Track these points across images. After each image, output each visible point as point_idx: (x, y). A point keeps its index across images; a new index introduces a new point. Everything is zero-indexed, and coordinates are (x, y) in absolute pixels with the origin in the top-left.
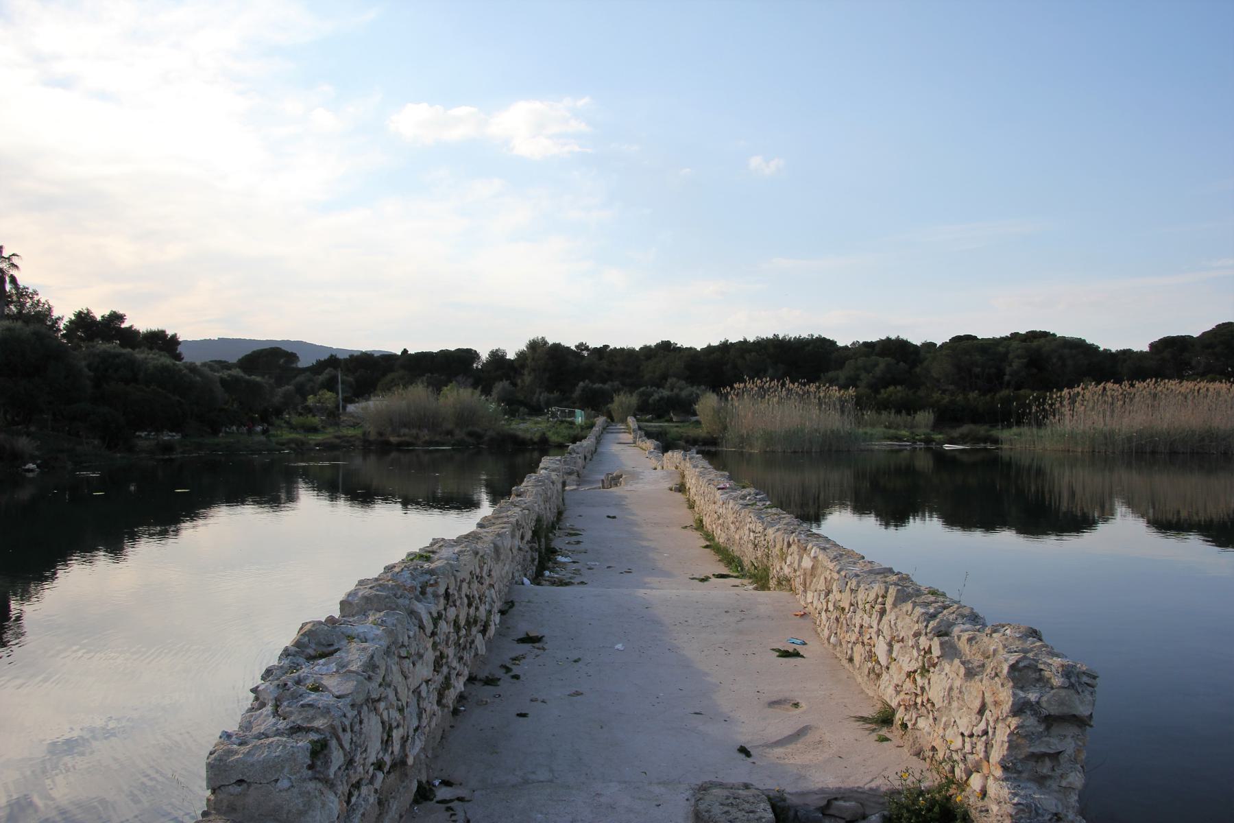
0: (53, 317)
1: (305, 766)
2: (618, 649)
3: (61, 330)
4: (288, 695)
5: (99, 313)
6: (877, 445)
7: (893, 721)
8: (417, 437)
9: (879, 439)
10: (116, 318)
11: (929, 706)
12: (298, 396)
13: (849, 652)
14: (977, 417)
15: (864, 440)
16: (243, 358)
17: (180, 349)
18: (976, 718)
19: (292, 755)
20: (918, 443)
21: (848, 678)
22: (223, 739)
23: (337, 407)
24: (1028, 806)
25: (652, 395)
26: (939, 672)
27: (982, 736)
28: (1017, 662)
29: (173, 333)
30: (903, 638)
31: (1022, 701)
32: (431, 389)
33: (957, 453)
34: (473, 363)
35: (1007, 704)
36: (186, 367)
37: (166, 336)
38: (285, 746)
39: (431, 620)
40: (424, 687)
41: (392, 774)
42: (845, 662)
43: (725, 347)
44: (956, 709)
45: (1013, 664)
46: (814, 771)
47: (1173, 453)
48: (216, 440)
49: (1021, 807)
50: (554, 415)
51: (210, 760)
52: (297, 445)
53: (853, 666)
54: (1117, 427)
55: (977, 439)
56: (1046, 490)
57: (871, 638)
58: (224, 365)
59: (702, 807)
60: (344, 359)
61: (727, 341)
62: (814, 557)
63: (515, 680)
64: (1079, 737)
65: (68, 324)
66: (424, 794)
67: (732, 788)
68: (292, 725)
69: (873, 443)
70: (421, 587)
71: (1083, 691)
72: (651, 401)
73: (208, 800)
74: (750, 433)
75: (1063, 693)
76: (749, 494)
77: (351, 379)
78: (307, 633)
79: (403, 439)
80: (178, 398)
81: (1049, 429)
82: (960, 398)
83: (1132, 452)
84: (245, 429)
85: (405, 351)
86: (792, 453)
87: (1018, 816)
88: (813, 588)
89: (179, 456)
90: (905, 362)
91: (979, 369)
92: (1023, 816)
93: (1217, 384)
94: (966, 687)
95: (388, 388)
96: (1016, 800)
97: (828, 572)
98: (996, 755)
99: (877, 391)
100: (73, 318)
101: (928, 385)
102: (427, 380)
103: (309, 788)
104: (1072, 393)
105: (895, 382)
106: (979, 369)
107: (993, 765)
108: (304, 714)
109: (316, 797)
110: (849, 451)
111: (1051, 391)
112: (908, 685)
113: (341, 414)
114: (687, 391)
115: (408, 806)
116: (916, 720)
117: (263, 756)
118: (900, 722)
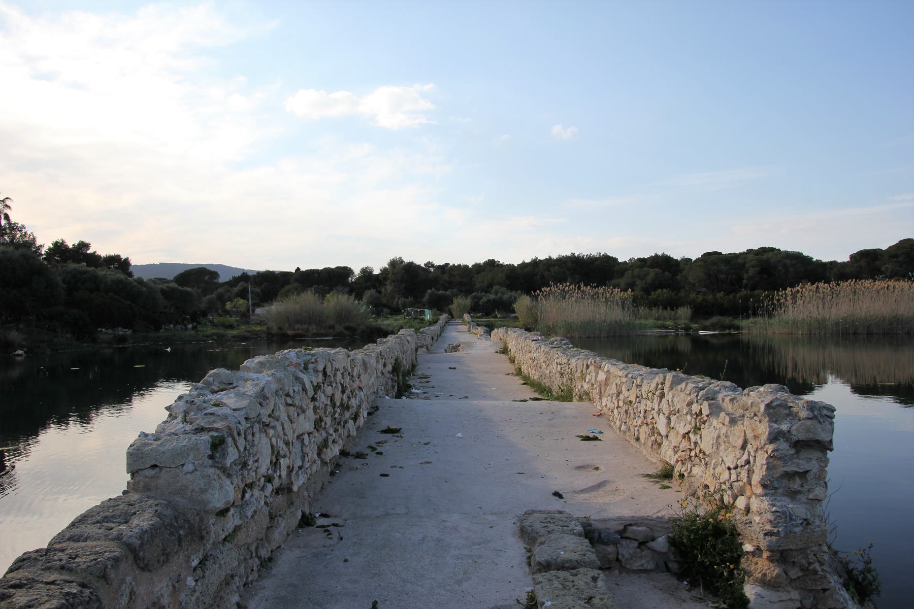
0: (37, 245)
1: (206, 455)
2: (458, 437)
3: (43, 255)
4: (194, 408)
5: (71, 242)
6: (649, 332)
7: (672, 475)
8: (307, 331)
9: (651, 328)
10: (83, 246)
11: (701, 455)
12: (219, 302)
13: (636, 434)
14: (722, 311)
15: (640, 329)
16: (178, 276)
17: (131, 269)
18: (740, 453)
19: (196, 445)
20: (680, 330)
21: (636, 452)
22: (141, 437)
23: (248, 310)
24: (784, 513)
25: (482, 298)
26: (708, 427)
27: (745, 466)
28: (772, 402)
29: (126, 257)
30: (679, 410)
31: (776, 431)
32: (317, 295)
33: (709, 338)
34: (349, 277)
35: (765, 434)
36: (135, 281)
37: (121, 259)
38: (190, 439)
39: (312, 387)
40: (306, 436)
41: (280, 496)
42: (633, 442)
43: (535, 263)
44: (723, 450)
45: (768, 403)
46: (613, 506)
47: (870, 334)
48: (158, 334)
49: (778, 514)
50: (409, 314)
51: (130, 450)
52: (218, 337)
53: (640, 444)
54: (828, 315)
55: (724, 327)
56: (776, 364)
57: (653, 418)
58: (163, 281)
59: (526, 523)
60: (253, 276)
61: (537, 258)
62: (608, 371)
63: (379, 455)
64: (822, 459)
65: (47, 251)
66: (306, 521)
67: (549, 513)
68: (197, 427)
69: (647, 331)
70: (304, 364)
71: (824, 422)
72: (481, 303)
73: (128, 483)
74: (555, 324)
75: (809, 422)
76: (556, 341)
77: (258, 290)
78: (213, 375)
79: (297, 332)
80: (129, 302)
81: (777, 318)
82: (710, 297)
83: (839, 334)
84: (179, 327)
85: (298, 269)
86: (586, 337)
87: (776, 522)
88: (607, 394)
89: (130, 345)
90: (669, 271)
91: (724, 276)
92: (780, 521)
93: (902, 283)
94: (731, 431)
95: (286, 295)
96: (774, 509)
97: (618, 378)
98: (756, 478)
99: (649, 294)
100: (52, 246)
101: (686, 289)
102: (315, 290)
103: (209, 472)
104: (793, 291)
105: (661, 286)
106: (724, 276)
107: (754, 486)
108: (207, 420)
109: (215, 480)
110: (628, 336)
111: (778, 291)
112: (684, 444)
113: (251, 315)
114: (508, 295)
115: (294, 528)
116: (691, 469)
117: (172, 446)
118: (678, 474)
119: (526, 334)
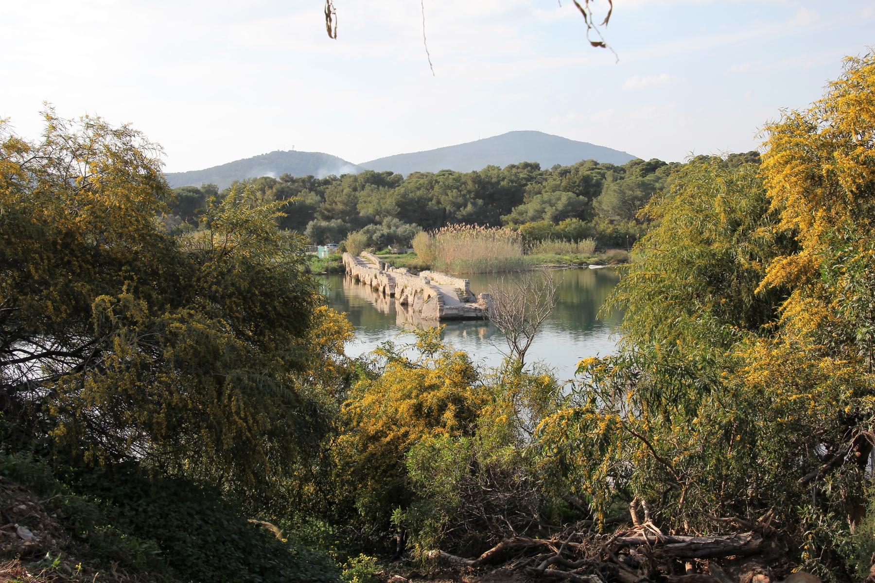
72: (374, 238)
101: (601, 216)
119: (13, 563)
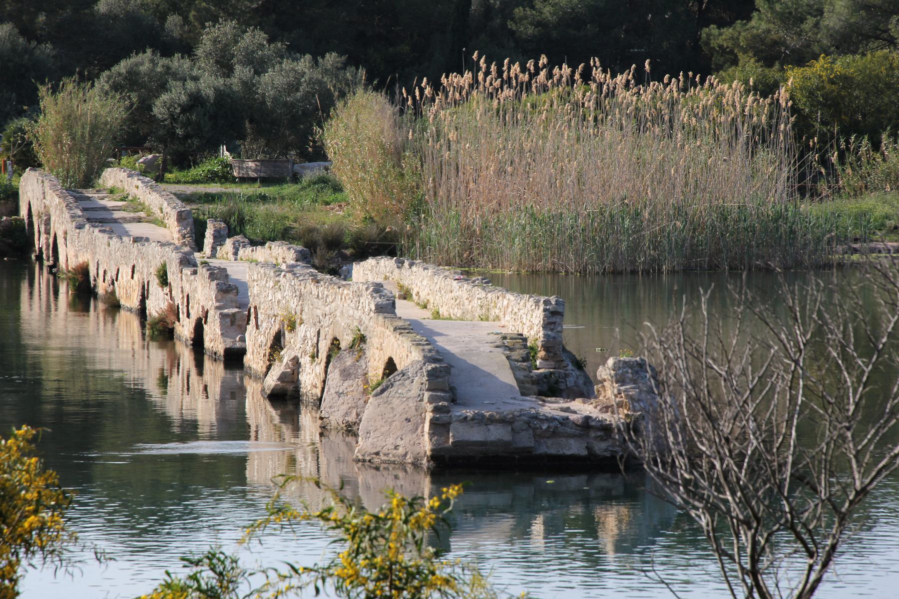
72: (159, 110)
